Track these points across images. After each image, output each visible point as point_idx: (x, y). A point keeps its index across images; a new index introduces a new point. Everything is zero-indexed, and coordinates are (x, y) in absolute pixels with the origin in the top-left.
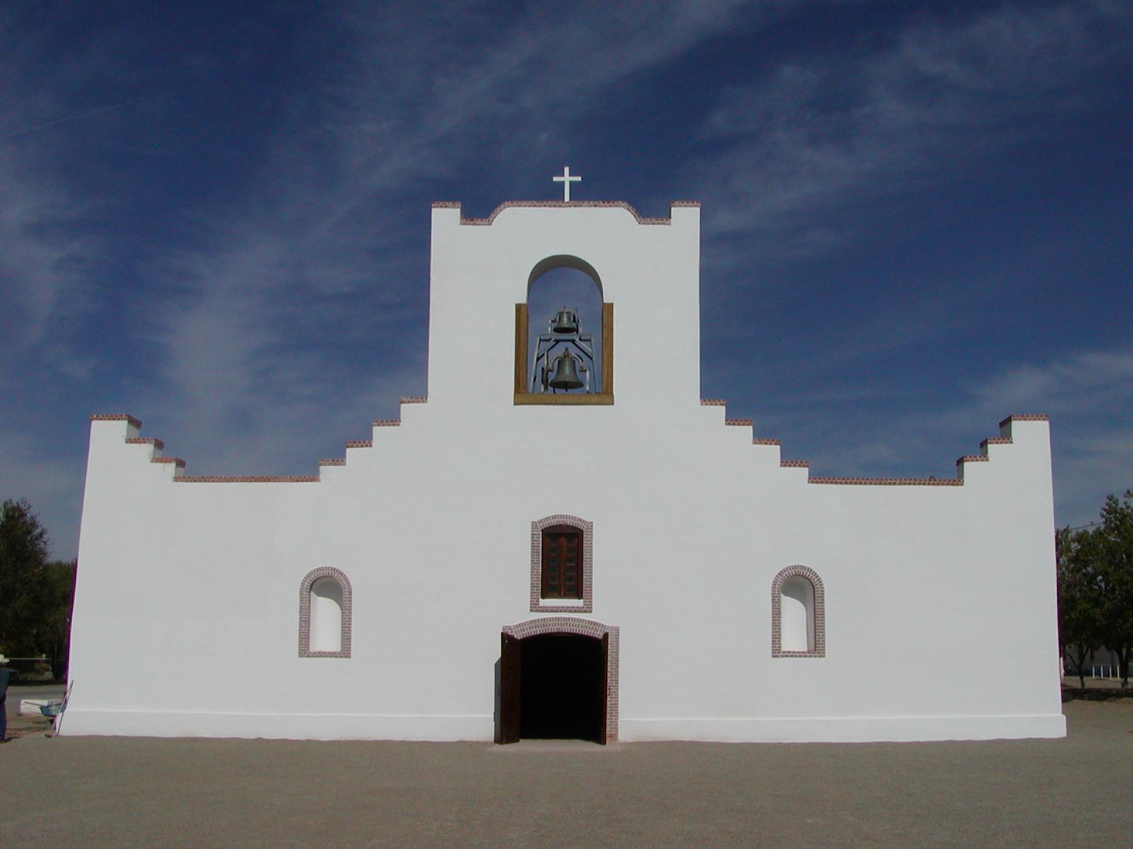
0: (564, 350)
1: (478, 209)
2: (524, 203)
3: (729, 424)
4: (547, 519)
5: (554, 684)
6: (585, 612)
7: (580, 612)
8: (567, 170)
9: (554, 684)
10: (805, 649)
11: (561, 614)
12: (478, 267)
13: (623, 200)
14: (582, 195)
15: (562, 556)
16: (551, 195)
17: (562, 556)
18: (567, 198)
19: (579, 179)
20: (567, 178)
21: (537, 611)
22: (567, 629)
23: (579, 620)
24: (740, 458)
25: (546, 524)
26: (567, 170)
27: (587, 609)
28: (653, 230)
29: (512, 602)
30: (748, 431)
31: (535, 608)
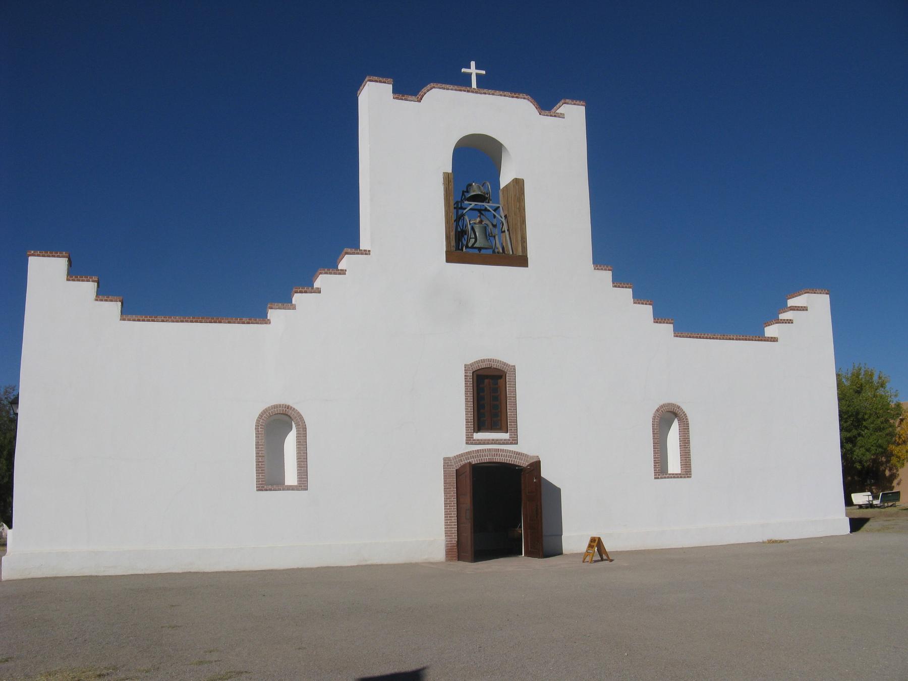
0: (481, 219)
1: (408, 87)
2: (410, 98)
3: (124, 320)
4: (477, 362)
5: (502, 508)
6: (511, 444)
7: (507, 444)
8: (473, 64)
9: (502, 508)
10: (679, 472)
11: (492, 445)
12: (403, 141)
13: (527, 94)
14: (485, 84)
15: (489, 395)
16: (463, 82)
17: (489, 395)
18: (474, 85)
19: (484, 72)
20: (473, 70)
21: (472, 444)
22: (498, 459)
23: (502, 450)
24: (627, 316)
25: (475, 368)
26: (473, 64)
27: (514, 441)
28: (547, 121)
29: (451, 435)
30: (628, 292)
31: (470, 441)
